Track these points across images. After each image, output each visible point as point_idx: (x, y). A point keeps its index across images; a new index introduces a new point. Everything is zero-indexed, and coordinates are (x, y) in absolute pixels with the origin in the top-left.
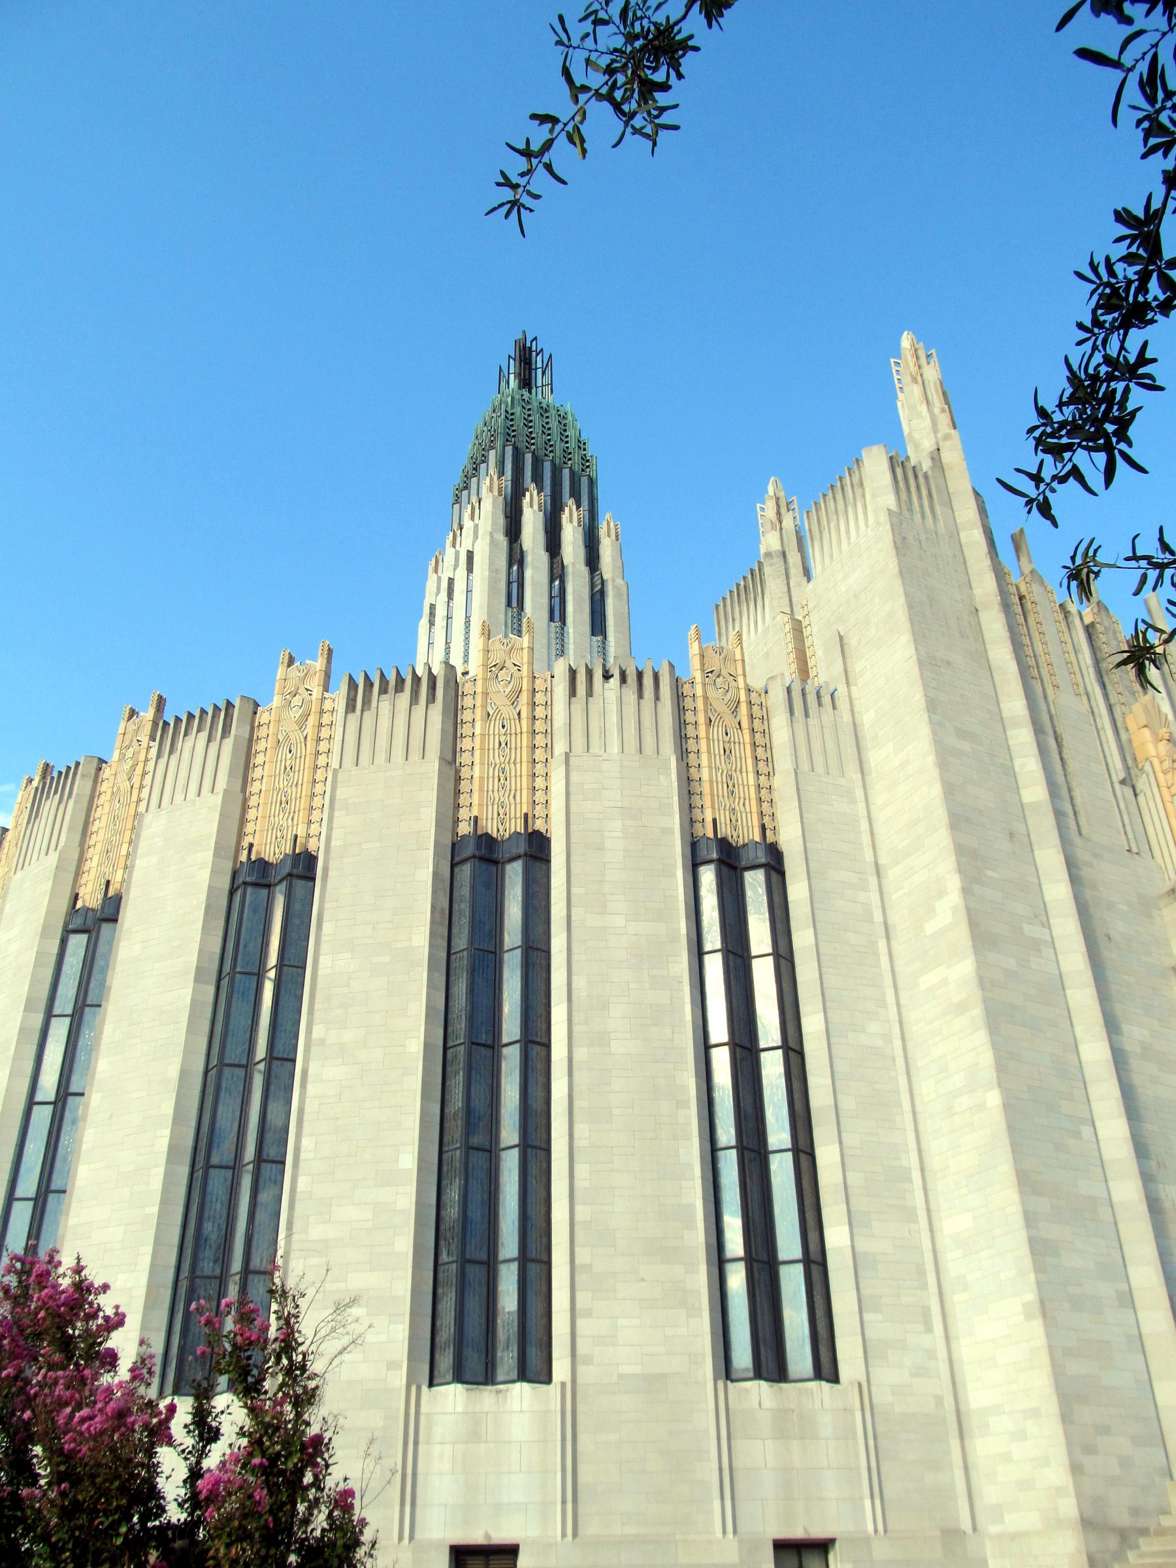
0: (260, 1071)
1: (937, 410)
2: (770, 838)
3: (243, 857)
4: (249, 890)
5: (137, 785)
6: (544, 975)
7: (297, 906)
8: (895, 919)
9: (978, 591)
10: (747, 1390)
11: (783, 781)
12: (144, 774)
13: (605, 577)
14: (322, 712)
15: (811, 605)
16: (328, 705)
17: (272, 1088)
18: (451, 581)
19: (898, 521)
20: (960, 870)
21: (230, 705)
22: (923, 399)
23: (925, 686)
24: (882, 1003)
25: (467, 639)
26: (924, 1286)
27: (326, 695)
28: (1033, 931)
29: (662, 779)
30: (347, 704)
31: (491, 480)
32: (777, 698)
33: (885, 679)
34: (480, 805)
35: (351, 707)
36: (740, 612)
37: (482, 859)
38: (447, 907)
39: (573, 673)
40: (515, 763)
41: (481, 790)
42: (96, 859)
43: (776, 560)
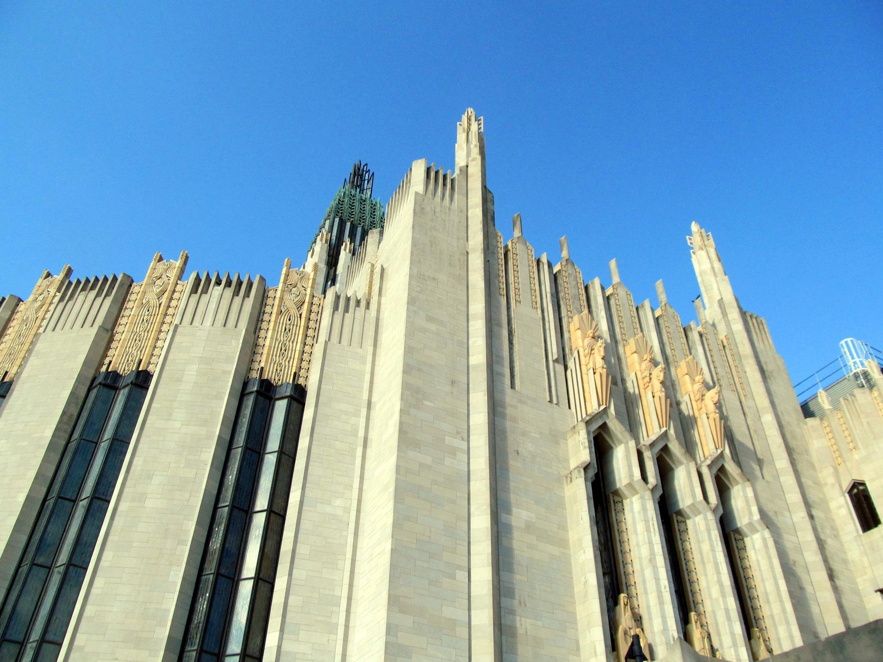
3: (104, 369)
16: (179, 288)
17: (88, 522)
21: (115, 279)
27: (179, 282)
34: (266, 362)
35: (194, 290)
39: (338, 297)
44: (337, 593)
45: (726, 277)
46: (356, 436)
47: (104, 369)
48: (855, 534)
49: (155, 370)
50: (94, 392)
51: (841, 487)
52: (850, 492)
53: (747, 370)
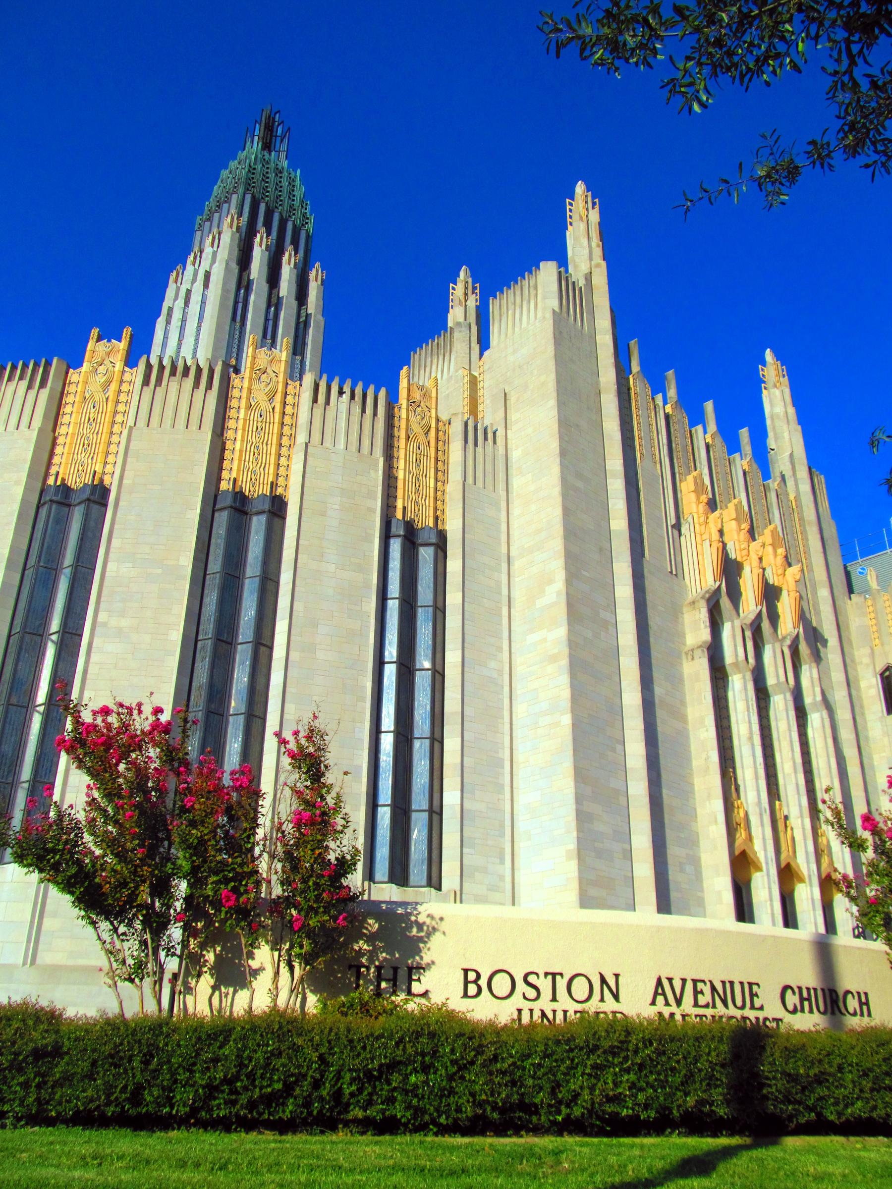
0: (53, 641)
1: (594, 244)
2: (440, 527)
4: (54, 506)
6: (273, 599)
8: (516, 594)
9: (602, 379)
10: (383, 889)
11: (453, 488)
13: (309, 312)
15: (486, 367)
18: (189, 292)
19: (558, 319)
20: (567, 568)
23: (561, 438)
24: (500, 649)
26: (502, 835)
28: (605, 615)
29: (372, 472)
30: (144, 379)
31: (232, 218)
32: (456, 429)
34: (239, 470)
35: (146, 382)
37: (236, 509)
40: (267, 444)
41: (240, 460)
43: (463, 329)
44: (500, 755)
45: (799, 427)
46: (500, 593)
47: (51, 481)
48: (880, 715)
50: (43, 512)
51: (875, 668)
52: (881, 675)
53: (810, 537)
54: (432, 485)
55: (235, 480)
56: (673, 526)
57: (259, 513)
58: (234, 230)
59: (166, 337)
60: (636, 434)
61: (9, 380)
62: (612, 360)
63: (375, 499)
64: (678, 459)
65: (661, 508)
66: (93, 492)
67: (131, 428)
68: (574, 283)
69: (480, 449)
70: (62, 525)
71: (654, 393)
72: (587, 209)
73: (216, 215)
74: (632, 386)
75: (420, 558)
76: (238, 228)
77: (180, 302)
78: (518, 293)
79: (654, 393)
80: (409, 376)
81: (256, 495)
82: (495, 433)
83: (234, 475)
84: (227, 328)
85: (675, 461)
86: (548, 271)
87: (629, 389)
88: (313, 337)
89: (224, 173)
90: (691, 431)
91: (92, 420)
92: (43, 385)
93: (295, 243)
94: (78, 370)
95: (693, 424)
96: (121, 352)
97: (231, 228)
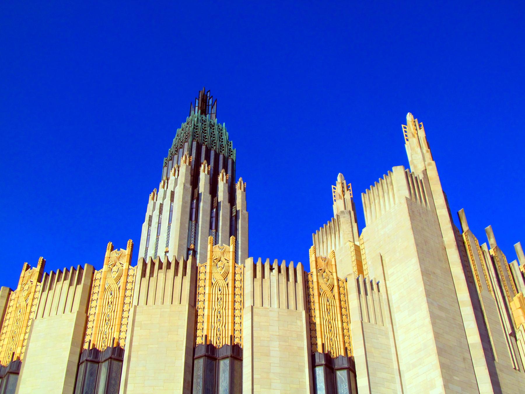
1: (424, 151)
4: (89, 364)
5: (30, 304)
7: (114, 375)
9: (445, 239)
11: (355, 327)
12: (34, 299)
13: (238, 209)
14: (128, 275)
15: (365, 240)
18: (161, 205)
19: (410, 203)
22: (418, 145)
23: (425, 284)
25: (168, 235)
29: (299, 323)
31: (186, 157)
32: (351, 285)
33: (403, 280)
34: (208, 329)
35: (143, 275)
36: (327, 239)
38: (191, 380)
41: (208, 322)
42: (6, 340)
43: (346, 215)
47: (86, 346)
49: (125, 344)
50: (82, 367)
54: (340, 326)
55: (206, 336)
56: (510, 335)
57: (224, 358)
58: (187, 164)
59: (149, 235)
60: (474, 273)
61: (58, 281)
62: (450, 225)
63: (303, 341)
64: (505, 286)
65: (499, 323)
66: (113, 353)
67: (135, 307)
68: (416, 178)
69: (369, 297)
70: (94, 376)
71: (481, 243)
72: (416, 130)
73: (176, 156)
74: (465, 240)
75: (338, 379)
76: (190, 163)
77: (157, 212)
78: (380, 189)
79: (481, 243)
80: (315, 253)
81: (221, 346)
82: (378, 284)
83: (205, 333)
84: (187, 225)
85: (503, 288)
86: (398, 171)
87: (464, 243)
88: (242, 225)
89: (179, 131)
90: (509, 265)
91: (110, 303)
92: (79, 282)
93: (225, 167)
94: (100, 271)
95: (510, 260)
96: (126, 256)
97: (186, 163)
